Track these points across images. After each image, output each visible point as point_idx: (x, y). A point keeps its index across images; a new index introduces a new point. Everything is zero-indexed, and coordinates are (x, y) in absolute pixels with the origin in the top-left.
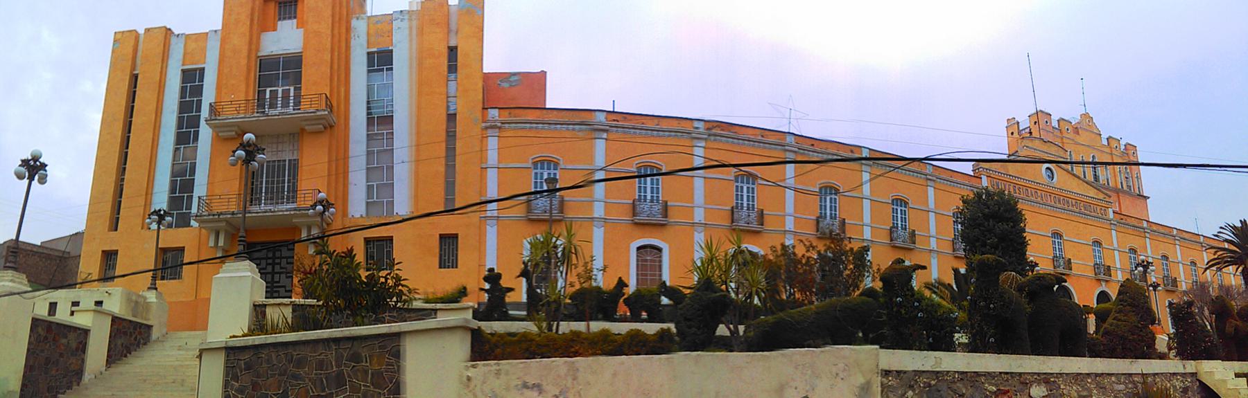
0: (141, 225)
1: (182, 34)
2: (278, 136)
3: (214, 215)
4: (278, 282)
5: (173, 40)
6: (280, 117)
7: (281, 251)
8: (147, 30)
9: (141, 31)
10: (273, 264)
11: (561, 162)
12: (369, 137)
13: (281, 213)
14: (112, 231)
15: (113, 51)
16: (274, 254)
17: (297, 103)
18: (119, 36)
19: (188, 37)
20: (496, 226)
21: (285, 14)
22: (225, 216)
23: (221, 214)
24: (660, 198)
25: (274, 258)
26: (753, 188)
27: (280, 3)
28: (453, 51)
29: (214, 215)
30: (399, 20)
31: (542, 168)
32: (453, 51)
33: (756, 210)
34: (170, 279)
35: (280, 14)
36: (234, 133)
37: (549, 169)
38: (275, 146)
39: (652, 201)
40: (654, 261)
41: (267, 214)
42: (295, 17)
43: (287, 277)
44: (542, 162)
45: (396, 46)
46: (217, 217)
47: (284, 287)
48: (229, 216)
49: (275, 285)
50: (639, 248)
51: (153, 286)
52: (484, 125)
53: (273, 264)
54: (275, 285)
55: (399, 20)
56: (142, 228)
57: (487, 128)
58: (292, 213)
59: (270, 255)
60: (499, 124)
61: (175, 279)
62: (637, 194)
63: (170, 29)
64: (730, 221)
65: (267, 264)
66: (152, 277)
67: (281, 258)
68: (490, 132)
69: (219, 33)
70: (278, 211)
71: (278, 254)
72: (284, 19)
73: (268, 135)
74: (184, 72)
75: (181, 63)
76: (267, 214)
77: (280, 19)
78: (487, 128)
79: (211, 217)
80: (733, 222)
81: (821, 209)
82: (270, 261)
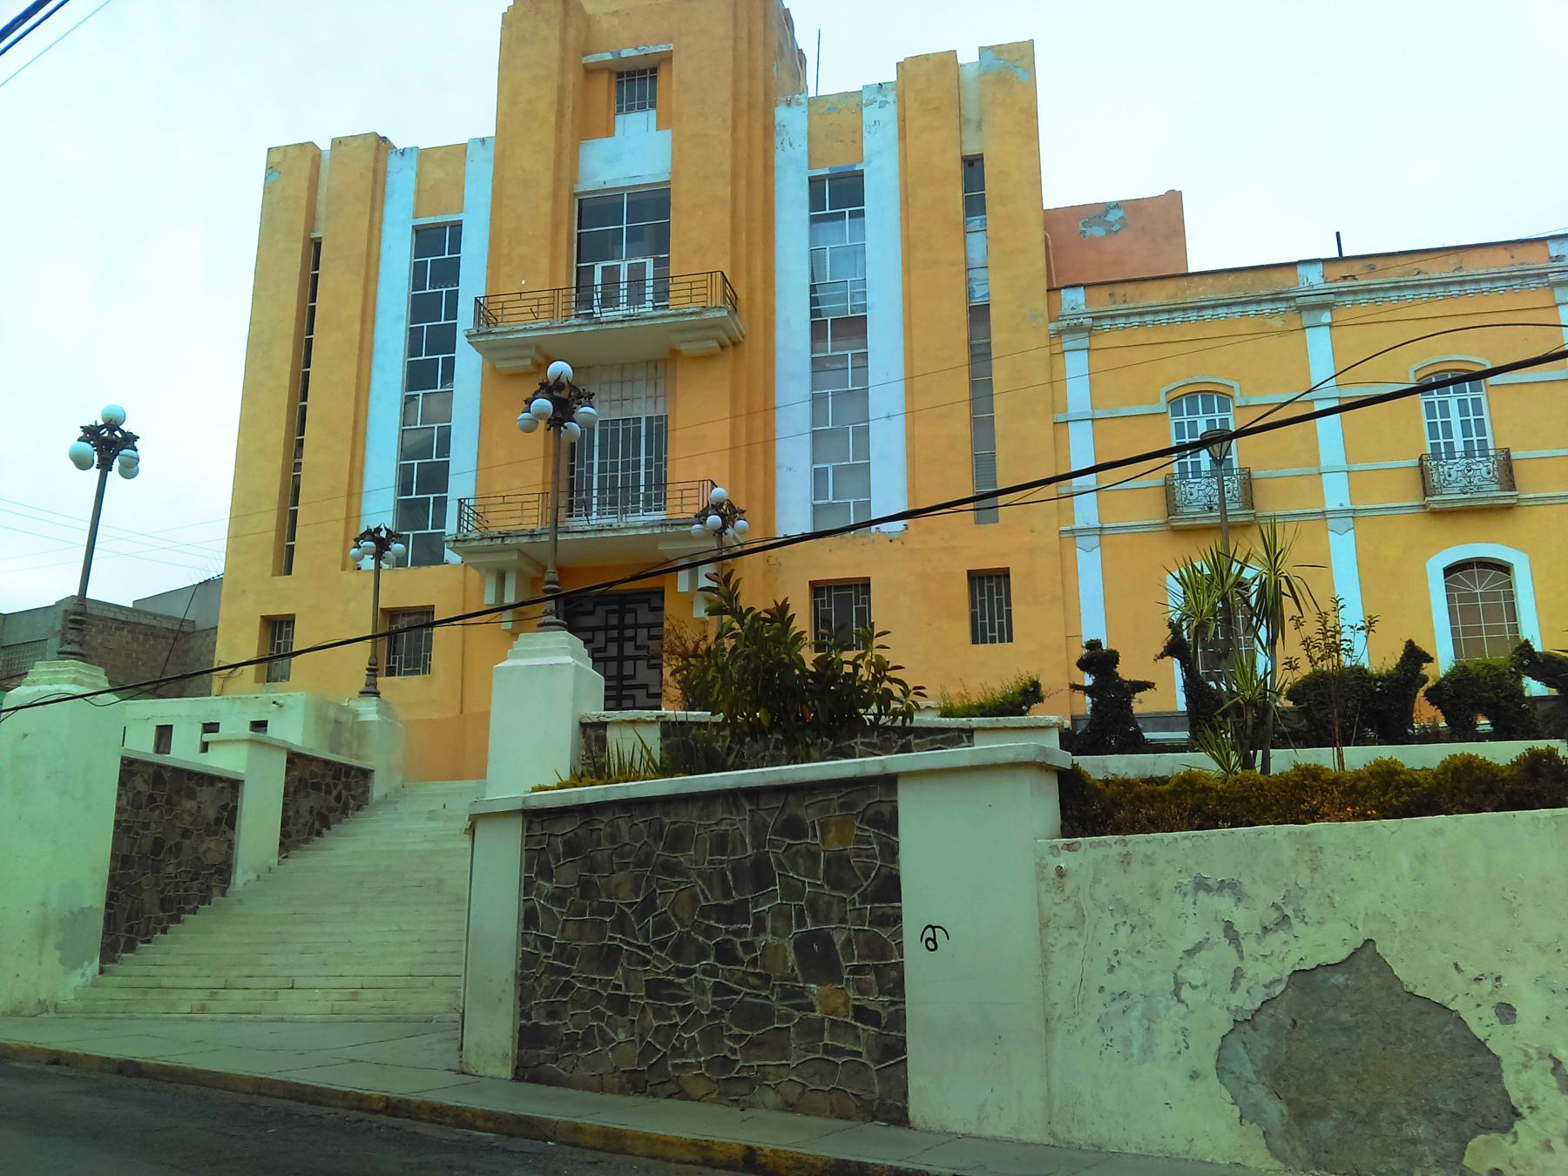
0: (340, 562)
1: (412, 149)
2: (622, 367)
3: (492, 538)
4: (633, 677)
5: (394, 162)
6: (626, 324)
7: (635, 611)
8: (337, 143)
9: (325, 145)
10: (621, 641)
11: (1237, 393)
12: (817, 365)
13: (632, 532)
14: (280, 574)
15: (267, 190)
16: (622, 619)
17: (662, 294)
18: (277, 158)
19: (424, 155)
20: (1099, 549)
21: (631, 98)
22: (514, 541)
23: (508, 535)
24: (1490, 445)
25: (621, 627)
26: (1476, 402)
27: (620, 75)
28: (973, 165)
29: (492, 538)
30: (877, 105)
31: (1193, 410)
32: (973, 165)
33: (1492, 453)
34: (406, 673)
35: (620, 101)
36: (529, 362)
37: (1208, 409)
38: (616, 387)
39: (1468, 453)
40: (1496, 596)
41: (604, 534)
42: (653, 105)
43: (650, 667)
44: (1191, 397)
45: (870, 162)
46: (499, 541)
47: (645, 686)
48: (525, 540)
49: (625, 683)
50: (1449, 571)
51: (371, 689)
52: (1053, 326)
53: (621, 641)
54: (625, 683)
55: (877, 105)
56: (343, 569)
57: (1059, 333)
58: (657, 531)
59: (614, 620)
60: (1088, 322)
61: (417, 672)
62: (1428, 441)
63: (385, 139)
64: (1162, 509)
65: (608, 640)
66: (367, 669)
67: (636, 626)
68: (1068, 342)
69: (491, 145)
70: (626, 528)
71: (629, 619)
72: (630, 109)
73: (602, 366)
74: (418, 231)
75: (410, 212)
76: (604, 534)
77: (620, 111)
78: (1059, 333)
79: (486, 542)
80: (1426, 495)
81: (1434, 435)
82: (614, 634)
